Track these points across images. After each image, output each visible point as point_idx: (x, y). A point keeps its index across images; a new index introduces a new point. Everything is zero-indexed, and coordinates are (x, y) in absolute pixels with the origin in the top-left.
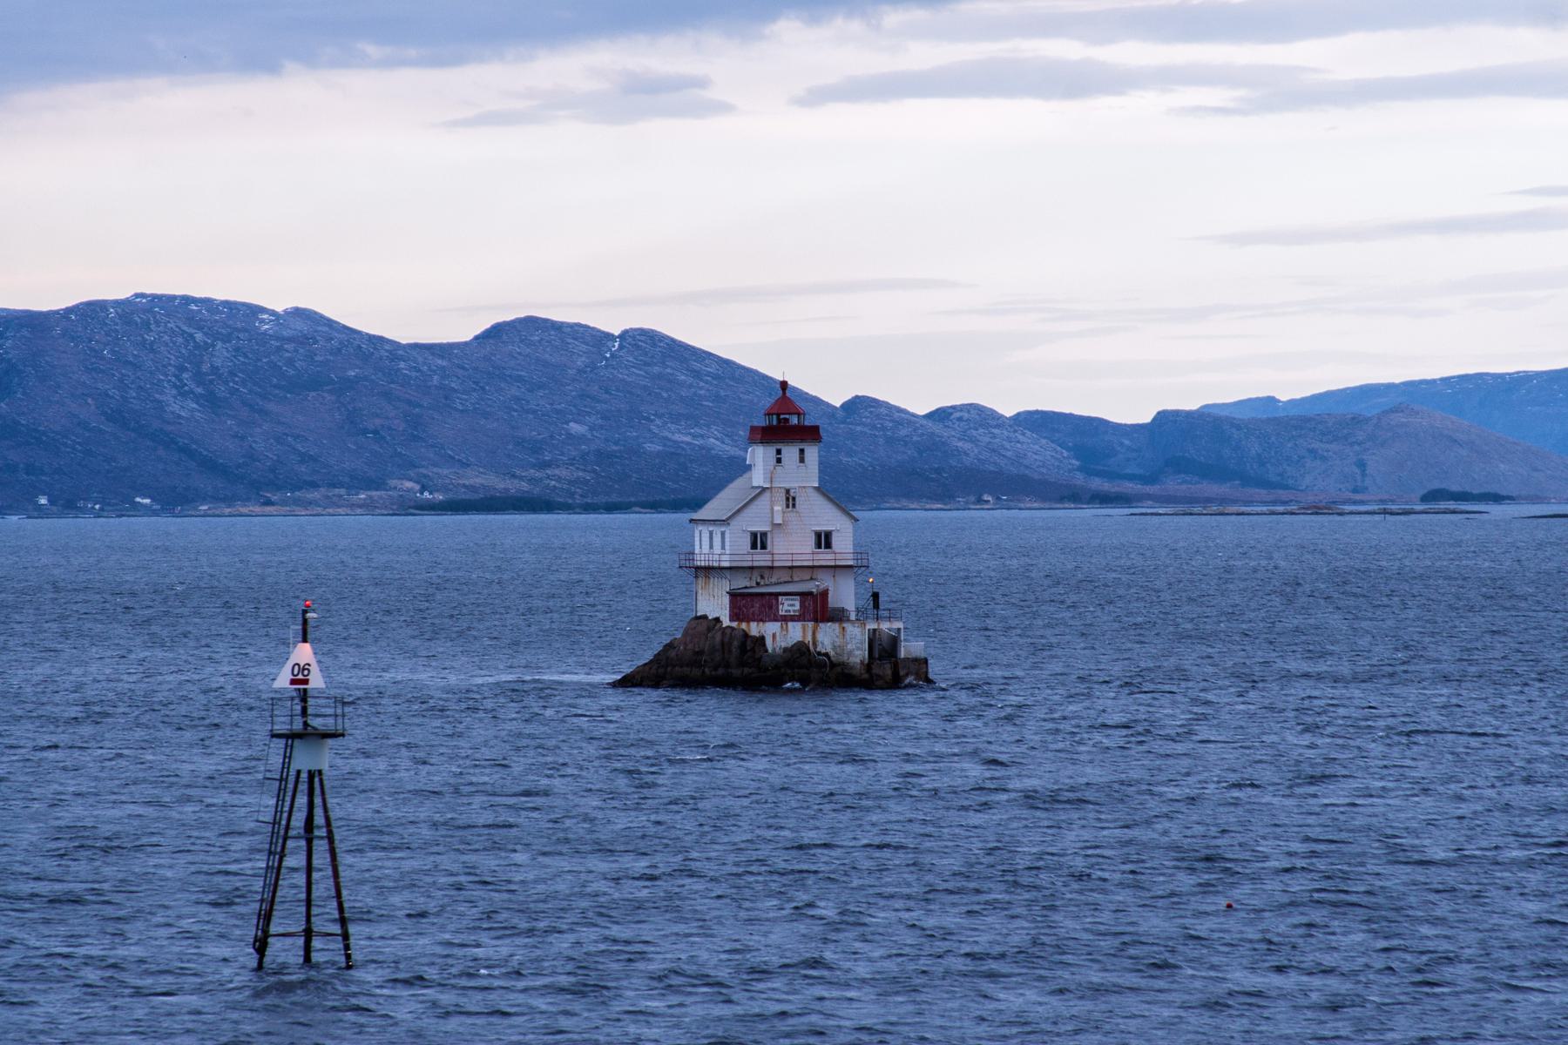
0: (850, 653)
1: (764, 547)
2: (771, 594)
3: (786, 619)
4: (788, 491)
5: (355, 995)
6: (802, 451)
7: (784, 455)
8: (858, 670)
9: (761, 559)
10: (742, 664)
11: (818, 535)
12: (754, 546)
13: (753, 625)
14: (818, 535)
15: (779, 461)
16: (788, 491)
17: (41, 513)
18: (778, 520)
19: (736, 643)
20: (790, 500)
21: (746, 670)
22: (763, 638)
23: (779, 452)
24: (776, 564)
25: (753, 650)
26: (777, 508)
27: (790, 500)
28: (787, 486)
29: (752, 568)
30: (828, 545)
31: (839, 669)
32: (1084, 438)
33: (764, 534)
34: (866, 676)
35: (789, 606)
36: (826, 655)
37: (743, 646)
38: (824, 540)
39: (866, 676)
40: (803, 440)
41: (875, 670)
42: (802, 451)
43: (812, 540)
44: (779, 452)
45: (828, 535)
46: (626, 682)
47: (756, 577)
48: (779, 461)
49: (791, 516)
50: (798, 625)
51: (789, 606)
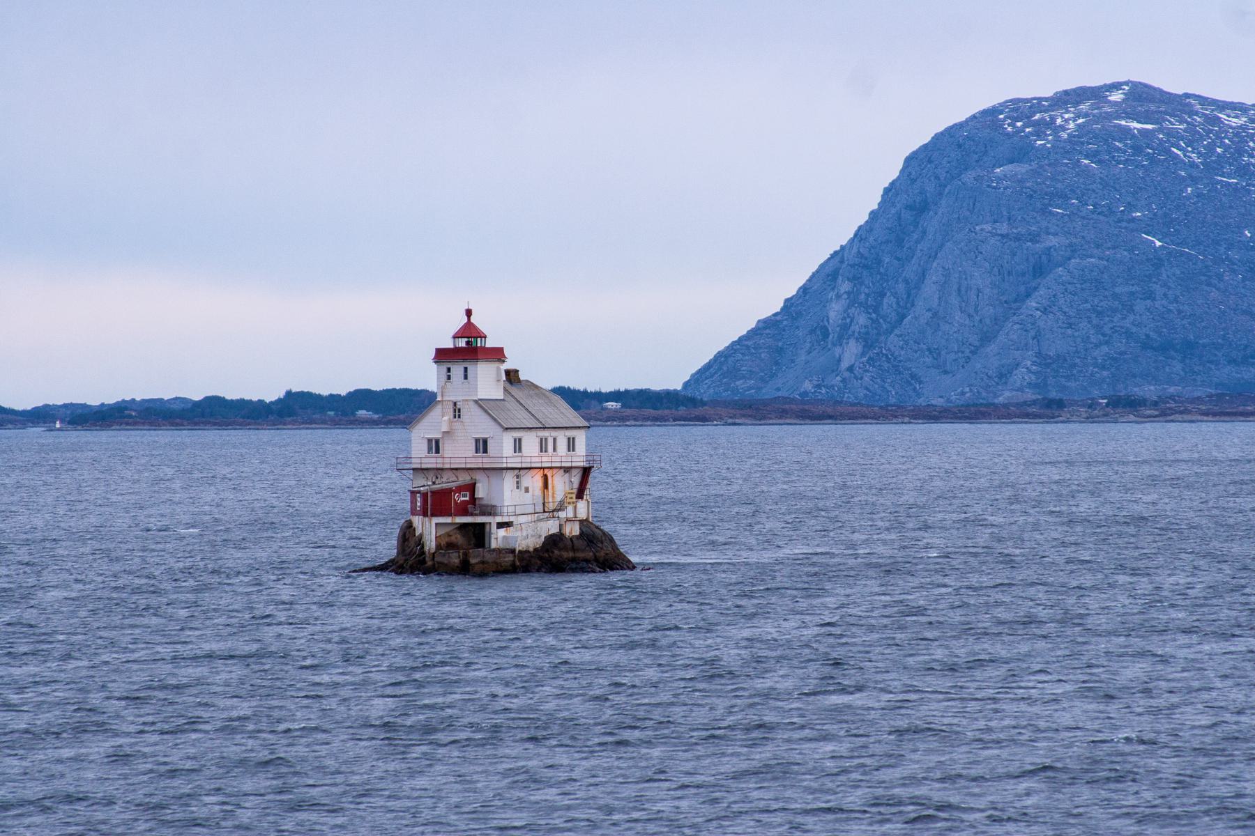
4: (455, 404)
7: (452, 374)
9: (431, 462)
11: (477, 441)
15: (449, 378)
16: (455, 404)
18: (445, 429)
20: (457, 413)
23: (449, 370)
28: (454, 399)
38: (482, 445)
40: (464, 360)
44: (449, 370)
45: (485, 442)
49: (457, 425)
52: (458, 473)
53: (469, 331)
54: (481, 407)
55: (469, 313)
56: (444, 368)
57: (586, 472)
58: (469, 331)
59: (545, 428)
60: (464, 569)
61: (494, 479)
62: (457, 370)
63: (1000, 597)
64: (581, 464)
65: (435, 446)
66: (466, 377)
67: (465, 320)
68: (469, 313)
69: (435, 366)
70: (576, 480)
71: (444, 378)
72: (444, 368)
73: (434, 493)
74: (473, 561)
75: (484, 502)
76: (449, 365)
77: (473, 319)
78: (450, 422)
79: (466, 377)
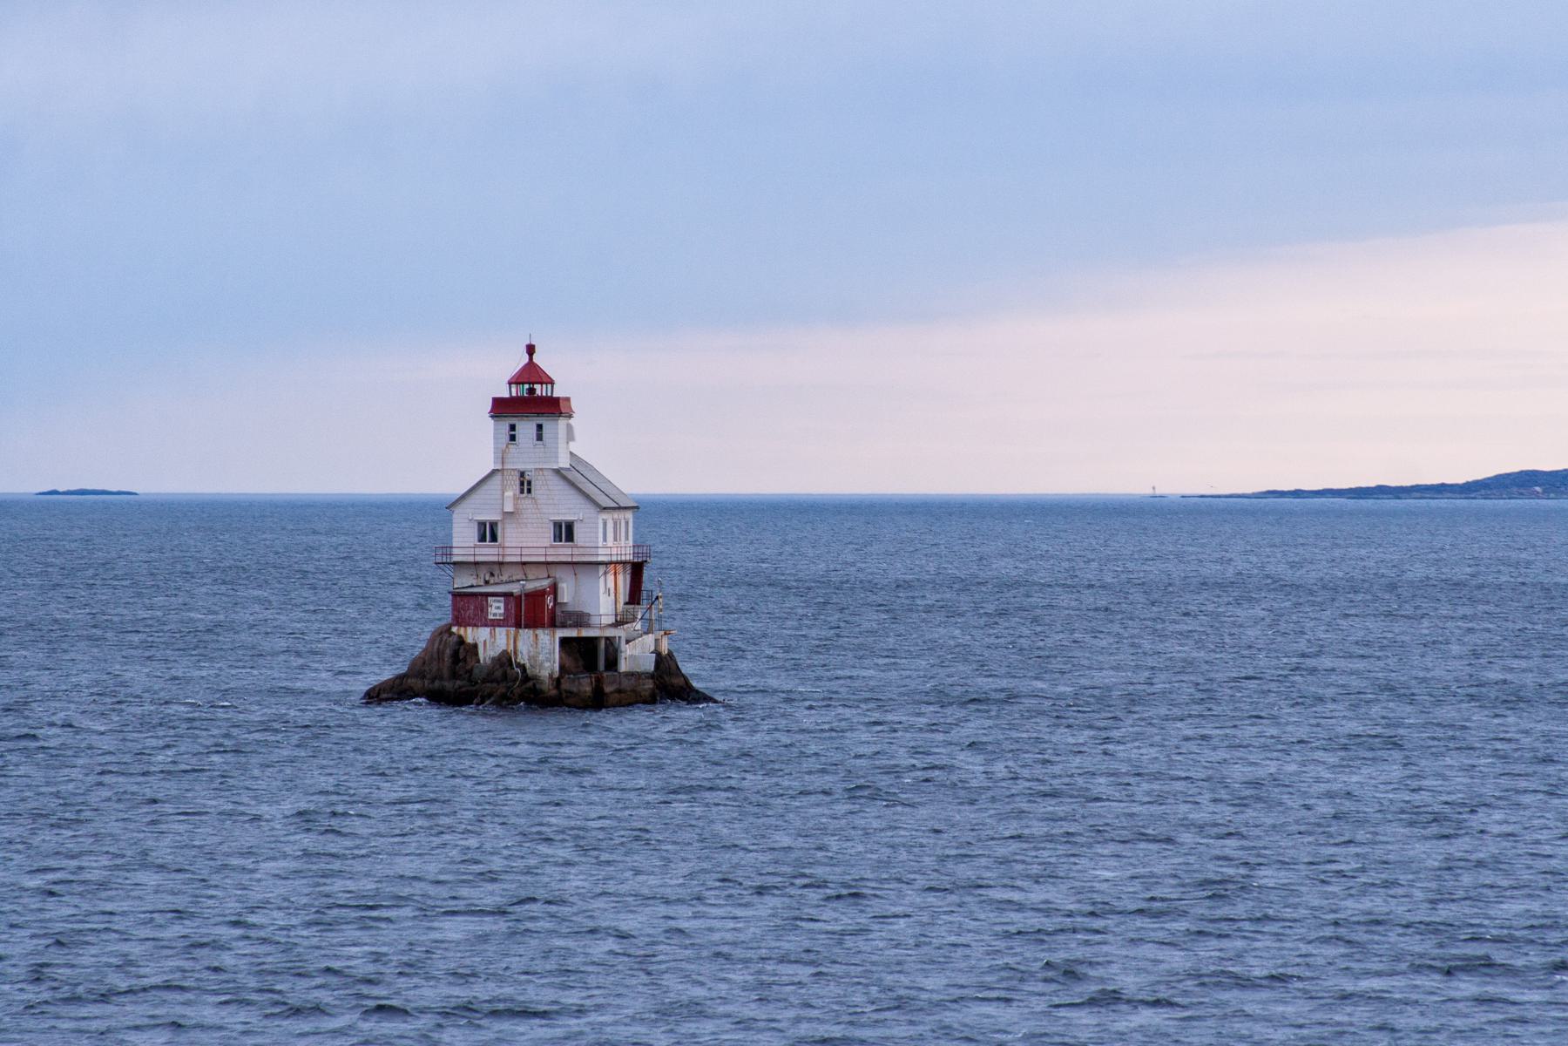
0: (541, 665)
1: (494, 538)
2: (482, 594)
3: (494, 624)
4: (522, 474)
5: (688, 960)
6: (540, 427)
7: (518, 432)
8: (546, 686)
9: (488, 553)
10: (454, 675)
11: (558, 525)
12: (482, 539)
13: (469, 629)
14: (558, 525)
15: (513, 438)
16: (522, 474)
17: (1537, 496)
18: (509, 508)
19: (448, 651)
20: (525, 485)
21: (459, 683)
22: (475, 646)
23: (513, 428)
24: (508, 559)
25: (465, 660)
26: (509, 494)
27: (525, 485)
28: (521, 467)
29: (476, 563)
30: (570, 538)
31: (530, 684)
32: (1368, 489)
33: (493, 525)
34: (554, 692)
35: (496, 609)
36: (523, 667)
37: (455, 654)
38: (565, 532)
39: (554, 692)
40: (539, 414)
41: (565, 686)
42: (540, 427)
43: (550, 532)
44: (513, 428)
45: (570, 527)
46: (375, 696)
47: (484, 573)
48: (513, 438)
49: (526, 503)
50: (503, 630)
51: (496, 609)
52: (527, 568)
53: (531, 374)
54: (565, 478)
55: (531, 350)
56: (504, 426)
57: (637, 569)
58: (531, 374)
59: (620, 508)
60: (598, 701)
61: (585, 579)
62: (526, 428)
63: (194, 761)
64: (629, 558)
65: (488, 532)
66: (540, 438)
67: (526, 359)
68: (531, 350)
69: (491, 422)
70: (624, 581)
71: (505, 438)
72: (504, 426)
73: (527, 595)
74: (608, 689)
75: (570, 609)
76: (513, 421)
77: (536, 359)
78: (516, 498)
79: (540, 438)
